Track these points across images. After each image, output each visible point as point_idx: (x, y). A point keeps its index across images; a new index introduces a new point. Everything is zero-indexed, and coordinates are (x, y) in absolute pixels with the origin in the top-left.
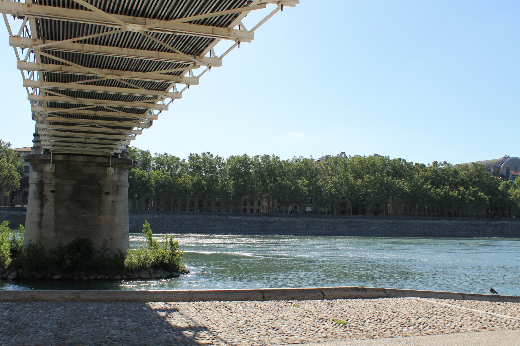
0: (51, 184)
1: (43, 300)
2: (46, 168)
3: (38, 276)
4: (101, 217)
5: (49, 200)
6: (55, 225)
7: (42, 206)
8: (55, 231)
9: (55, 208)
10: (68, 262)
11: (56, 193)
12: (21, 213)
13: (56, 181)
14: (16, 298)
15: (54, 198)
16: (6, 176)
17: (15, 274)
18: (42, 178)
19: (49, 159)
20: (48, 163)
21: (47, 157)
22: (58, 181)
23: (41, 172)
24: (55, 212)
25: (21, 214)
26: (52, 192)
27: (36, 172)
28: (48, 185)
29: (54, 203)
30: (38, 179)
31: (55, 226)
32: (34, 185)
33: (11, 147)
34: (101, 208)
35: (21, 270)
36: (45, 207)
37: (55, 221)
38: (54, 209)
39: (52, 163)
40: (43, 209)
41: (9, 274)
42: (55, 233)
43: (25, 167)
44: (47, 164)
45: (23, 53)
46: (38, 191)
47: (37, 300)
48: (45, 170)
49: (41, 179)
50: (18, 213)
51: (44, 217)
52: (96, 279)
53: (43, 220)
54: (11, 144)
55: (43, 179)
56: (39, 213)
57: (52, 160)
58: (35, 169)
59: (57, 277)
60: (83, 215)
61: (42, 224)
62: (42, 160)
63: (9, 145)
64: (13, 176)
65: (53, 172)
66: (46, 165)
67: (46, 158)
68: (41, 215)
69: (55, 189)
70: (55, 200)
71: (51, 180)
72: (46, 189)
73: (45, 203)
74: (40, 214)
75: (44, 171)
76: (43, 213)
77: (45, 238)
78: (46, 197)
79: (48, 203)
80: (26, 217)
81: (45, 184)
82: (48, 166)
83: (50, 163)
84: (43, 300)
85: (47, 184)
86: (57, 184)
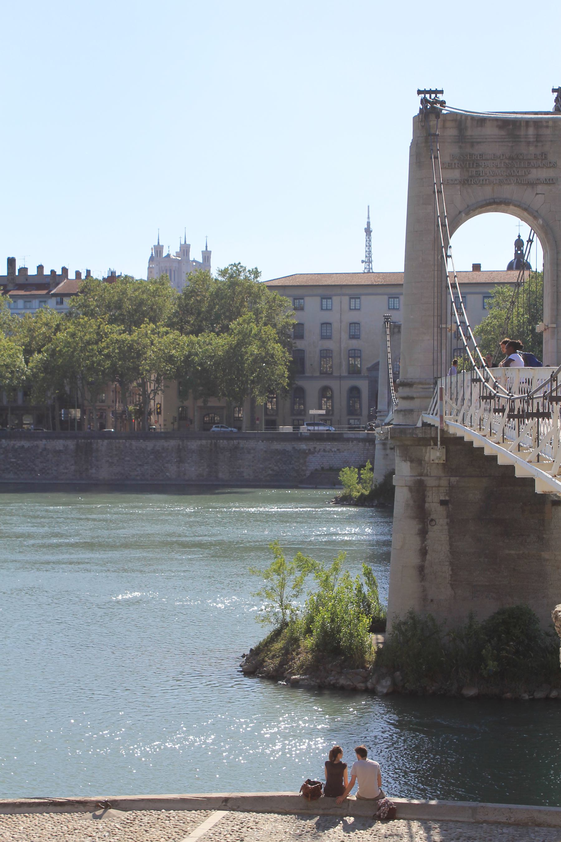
0: (439, 486)
1: (549, 826)
2: (428, 455)
3: (433, 688)
4: (546, 555)
5: (437, 521)
6: (451, 573)
7: (423, 533)
8: (451, 585)
9: (450, 538)
10: (492, 665)
11: (450, 506)
12: (295, 446)
13: (449, 480)
14: (510, 820)
15: (448, 517)
16: (256, 357)
17: (389, 683)
18: (421, 475)
19: (433, 436)
20: (432, 443)
21: (431, 433)
22: (453, 479)
23: (417, 462)
24: (451, 545)
25: (294, 448)
26: (443, 503)
27: (409, 463)
28: (434, 489)
29: (446, 527)
30: (413, 478)
31: (451, 575)
32: (405, 491)
33: (261, 279)
34: (545, 536)
35: (398, 673)
36: (430, 534)
37: (451, 564)
38: (448, 539)
39: (441, 444)
40: (426, 541)
41: (378, 682)
42: (452, 588)
43: (294, 325)
44: (430, 445)
45: (369, 207)
46: (415, 502)
47: (539, 825)
48: (427, 459)
49: (419, 478)
50: (288, 446)
51: (428, 557)
52: (547, 699)
53: (427, 564)
54: (259, 271)
55: (423, 478)
56: (419, 548)
57: (441, 438)
58: (407, 457)
59: (471, 692)
60: (507, 552)
61: (426, 571)
62: (420, 439)
63: (256, 273)
64: (272, 356)
65: (442, 462)
66: (429, 447)
67: (428, 436)
68: (424, 552)
69: (447, 498)
70: (448, 520)
71: (439, 478)
72: (430, 497)
73: (429, 526)
74: (420, 550)
75: (424, 461)
76: (427, 548)
77: (432, 600)
78: (430, 514)
79: (435, 527)
80: (391, 556)
81: (428, 489)
82: (432, 451)
83: (436, 444)
84: (549, 826)
85: (432, 487)
86: (451, 487)
